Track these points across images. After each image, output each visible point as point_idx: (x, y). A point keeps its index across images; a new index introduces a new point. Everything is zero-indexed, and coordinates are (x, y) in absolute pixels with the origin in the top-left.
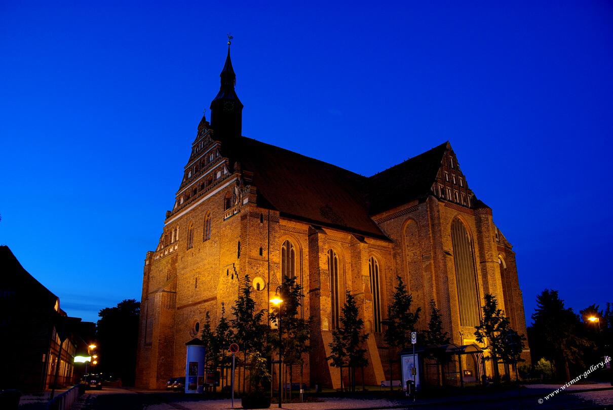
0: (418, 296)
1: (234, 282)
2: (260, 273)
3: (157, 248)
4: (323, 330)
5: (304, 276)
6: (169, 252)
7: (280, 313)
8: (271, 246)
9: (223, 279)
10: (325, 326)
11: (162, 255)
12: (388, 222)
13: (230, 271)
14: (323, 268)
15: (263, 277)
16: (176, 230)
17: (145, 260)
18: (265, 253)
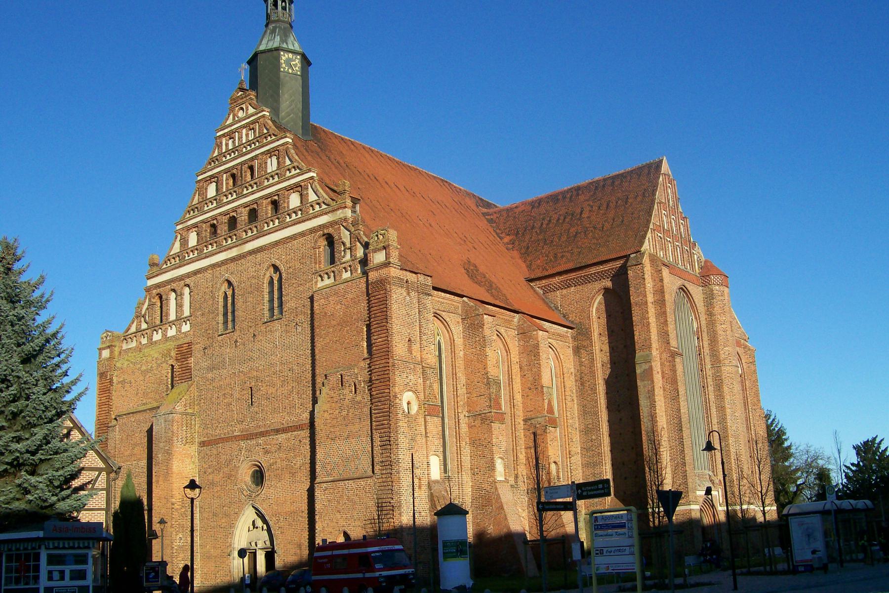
0: (621, 419)
1: (359, 398)
2: (410, 384)
3: (130, 326)
4: (498, 479)
5: (459, 387)
6: (164, 335)
7: (800, 500)
8: (424, 337)
9: (332, 393)
10: (500, 472)
11: (144, 341)
12: (565, 291)
13: (346, 378)
14: (492, 373)
15: (415, 392)
16: (179, 295)
17: (100, 350)
18: (416, 347)
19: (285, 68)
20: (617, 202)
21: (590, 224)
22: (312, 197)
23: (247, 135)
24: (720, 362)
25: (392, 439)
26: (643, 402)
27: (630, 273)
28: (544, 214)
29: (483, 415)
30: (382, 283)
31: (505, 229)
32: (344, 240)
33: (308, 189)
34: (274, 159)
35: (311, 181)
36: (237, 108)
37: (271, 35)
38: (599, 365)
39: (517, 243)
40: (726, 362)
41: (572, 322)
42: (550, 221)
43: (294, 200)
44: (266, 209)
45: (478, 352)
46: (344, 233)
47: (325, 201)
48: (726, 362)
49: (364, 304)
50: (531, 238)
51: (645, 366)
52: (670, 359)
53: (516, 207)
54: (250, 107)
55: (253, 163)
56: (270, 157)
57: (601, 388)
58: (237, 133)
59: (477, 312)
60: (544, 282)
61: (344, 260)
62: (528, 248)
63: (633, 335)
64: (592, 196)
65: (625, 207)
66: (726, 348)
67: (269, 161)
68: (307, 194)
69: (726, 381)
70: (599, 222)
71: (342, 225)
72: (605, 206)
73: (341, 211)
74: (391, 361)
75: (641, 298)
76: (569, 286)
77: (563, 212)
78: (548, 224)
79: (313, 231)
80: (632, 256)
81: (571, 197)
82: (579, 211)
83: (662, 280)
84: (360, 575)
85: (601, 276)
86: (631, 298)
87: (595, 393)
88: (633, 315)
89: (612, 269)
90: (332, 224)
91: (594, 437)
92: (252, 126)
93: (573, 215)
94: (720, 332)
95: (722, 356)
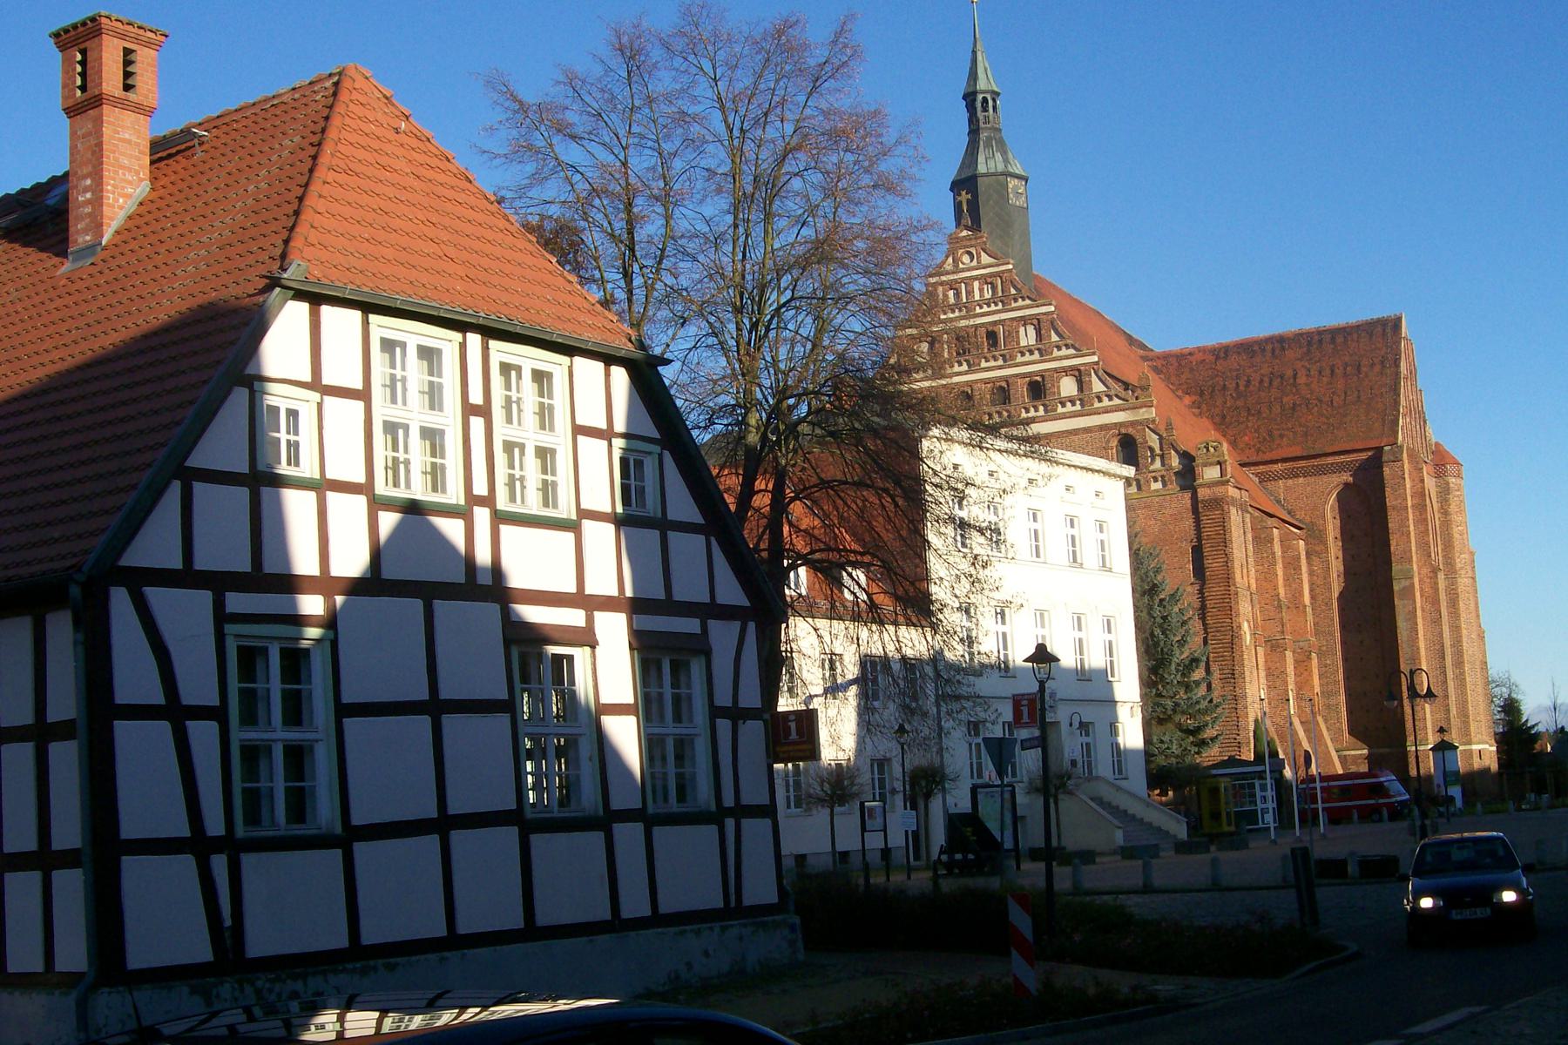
0: (1361, 642)
12: (1290, 482)
19: (1012, 200)
20: (1345, 369)
21: (1311, 394)
22: (1098, 387)
23: (981, 290)
24: (1455, 572)
25: (1236, 672)
26: (1402, 624)
27: (1386, 471)
28: (1238, 370)
29: (1274, 642)
30: (1218, 503)
31: (1180, 385)
32: (1150, 444)
33: (1090, 375)
34: (1031, 330)
35: (1095, 367)
36: (960, 251)
37: (987, 150)
38: (1335, 575)
39: (1204, 407)
40: (1463, 572)
41: (1300, 521)
42: (1248, 382)
43: (1068, 387)
44: (1021, 391)
45: (1266, 570)
46: (1150, 437)
47: (1119, 394)
48: (1463, 572)
49: (1189, 523)
50: (1225, 403)
51: (1405, 583)
52: (1432, 575)
53: (1190, 354)
54: (983, 253)
55: (995, 329)
56: (1025, 325)
57: (1335, 605)
58: (963, 284)
59: (1264, 524)
60: (1261, 467)
61: (1152, 468)
62: (1224, 417)
63: (1389, 546)
64: (1305, 354)
65: (1359, 378)
66: (1463, 556)
67: (1022, 330)
68: (1090, 381)
69: (1461, 596)
70: (1325, 395)
71: (1148, 427)
72: (1328, 372)
73: (1144, 409)
74: (1232, 588)
75: (1399, 501)
76: (1297, 476)
77: (1266, 370)
78: (1247, 386)
79: (1102, 428)
80: (1386, 448)
81: (1273, 350)
82: (1289, 373)
83: (1422, 481)
84: (1372, 802)
85: (1340, 468)
86: (1387, 500)
87: (1330, 609)
88: (1389, 521)
89: (1357, 461)
90: (1133, 424)
91: (1328, 662)
92: (989, 280)
93: (1282, 378)
94: (1456, 536)
95: (1459, 566)
